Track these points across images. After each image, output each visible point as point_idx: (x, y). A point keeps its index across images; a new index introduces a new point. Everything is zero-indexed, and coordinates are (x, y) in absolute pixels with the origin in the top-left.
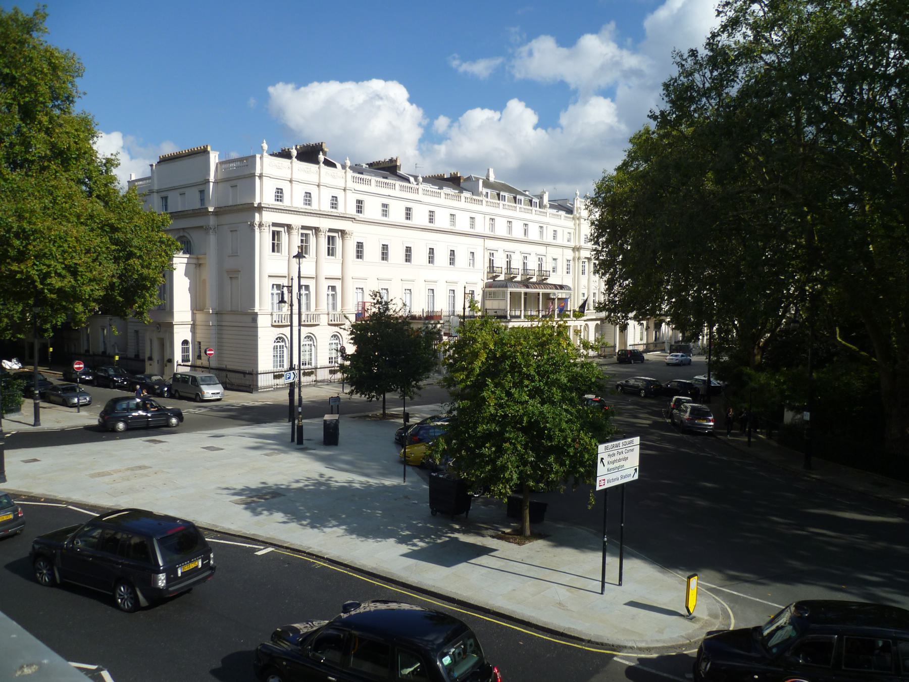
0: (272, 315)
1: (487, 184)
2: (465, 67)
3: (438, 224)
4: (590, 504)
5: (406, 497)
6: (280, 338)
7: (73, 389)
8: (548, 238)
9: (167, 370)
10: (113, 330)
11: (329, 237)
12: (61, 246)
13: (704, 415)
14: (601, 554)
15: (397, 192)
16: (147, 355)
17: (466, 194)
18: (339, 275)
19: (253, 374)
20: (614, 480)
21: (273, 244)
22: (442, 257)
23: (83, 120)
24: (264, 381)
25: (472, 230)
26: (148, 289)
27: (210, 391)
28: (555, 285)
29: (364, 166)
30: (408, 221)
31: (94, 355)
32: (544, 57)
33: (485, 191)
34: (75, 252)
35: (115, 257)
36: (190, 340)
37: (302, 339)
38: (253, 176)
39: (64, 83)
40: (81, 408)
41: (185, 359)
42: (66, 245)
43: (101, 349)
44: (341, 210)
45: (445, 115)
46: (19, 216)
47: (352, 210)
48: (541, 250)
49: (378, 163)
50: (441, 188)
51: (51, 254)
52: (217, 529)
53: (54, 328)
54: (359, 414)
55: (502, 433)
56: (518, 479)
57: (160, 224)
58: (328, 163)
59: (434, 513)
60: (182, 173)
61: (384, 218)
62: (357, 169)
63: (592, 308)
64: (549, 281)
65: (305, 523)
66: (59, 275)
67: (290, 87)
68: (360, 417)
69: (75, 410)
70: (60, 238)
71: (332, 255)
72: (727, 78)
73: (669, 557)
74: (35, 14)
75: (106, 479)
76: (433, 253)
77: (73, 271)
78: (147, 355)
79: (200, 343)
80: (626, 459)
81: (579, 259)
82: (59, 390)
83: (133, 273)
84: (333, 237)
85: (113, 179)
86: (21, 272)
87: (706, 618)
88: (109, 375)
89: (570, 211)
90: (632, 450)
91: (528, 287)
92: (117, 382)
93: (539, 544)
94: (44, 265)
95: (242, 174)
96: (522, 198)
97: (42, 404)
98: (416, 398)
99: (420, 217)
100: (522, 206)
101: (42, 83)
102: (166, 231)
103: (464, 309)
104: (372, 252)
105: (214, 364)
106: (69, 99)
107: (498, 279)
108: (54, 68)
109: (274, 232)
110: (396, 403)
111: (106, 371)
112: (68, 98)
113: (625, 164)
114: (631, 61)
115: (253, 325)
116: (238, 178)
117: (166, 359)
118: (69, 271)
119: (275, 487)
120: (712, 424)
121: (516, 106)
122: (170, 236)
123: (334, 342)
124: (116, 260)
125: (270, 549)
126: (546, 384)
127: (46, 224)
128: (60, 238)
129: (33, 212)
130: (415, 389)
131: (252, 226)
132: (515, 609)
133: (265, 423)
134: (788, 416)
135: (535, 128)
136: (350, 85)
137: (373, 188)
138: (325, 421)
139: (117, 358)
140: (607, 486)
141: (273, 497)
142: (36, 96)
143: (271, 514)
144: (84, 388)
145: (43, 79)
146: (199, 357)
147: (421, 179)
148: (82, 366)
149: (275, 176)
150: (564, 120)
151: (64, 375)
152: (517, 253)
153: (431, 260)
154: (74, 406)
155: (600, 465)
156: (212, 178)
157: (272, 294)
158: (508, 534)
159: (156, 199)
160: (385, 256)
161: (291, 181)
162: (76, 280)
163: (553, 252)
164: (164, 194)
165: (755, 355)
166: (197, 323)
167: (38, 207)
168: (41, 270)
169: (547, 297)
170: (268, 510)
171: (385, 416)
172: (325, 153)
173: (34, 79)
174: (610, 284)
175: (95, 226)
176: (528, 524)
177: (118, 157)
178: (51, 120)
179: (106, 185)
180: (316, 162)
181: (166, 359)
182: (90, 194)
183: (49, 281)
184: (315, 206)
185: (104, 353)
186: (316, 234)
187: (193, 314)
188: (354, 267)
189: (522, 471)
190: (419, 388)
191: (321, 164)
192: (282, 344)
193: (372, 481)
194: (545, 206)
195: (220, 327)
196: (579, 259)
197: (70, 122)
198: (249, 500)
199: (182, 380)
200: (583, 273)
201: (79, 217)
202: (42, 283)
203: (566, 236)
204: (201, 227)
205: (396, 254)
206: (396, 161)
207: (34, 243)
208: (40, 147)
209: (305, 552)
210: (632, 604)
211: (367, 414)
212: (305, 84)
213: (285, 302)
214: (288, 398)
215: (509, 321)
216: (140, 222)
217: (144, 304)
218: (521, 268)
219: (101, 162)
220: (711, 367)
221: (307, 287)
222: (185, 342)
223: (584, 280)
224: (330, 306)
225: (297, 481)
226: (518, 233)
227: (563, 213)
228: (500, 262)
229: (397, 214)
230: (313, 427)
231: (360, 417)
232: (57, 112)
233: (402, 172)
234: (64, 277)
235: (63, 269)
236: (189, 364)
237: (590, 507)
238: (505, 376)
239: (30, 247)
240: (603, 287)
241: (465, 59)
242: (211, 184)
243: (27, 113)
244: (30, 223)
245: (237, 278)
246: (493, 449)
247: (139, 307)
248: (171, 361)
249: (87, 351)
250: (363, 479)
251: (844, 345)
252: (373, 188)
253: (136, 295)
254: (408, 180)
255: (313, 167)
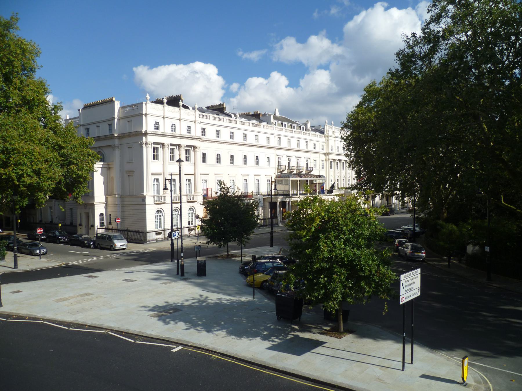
0: (154, 197)
1: (275, 118)
2: (246, 56)
3: (248, 141)
4: (385, 311)
5: (258, 309)
6: (159, 211)
7: (36, 245)
8: (311, 148)
9: (91, 231)
10: (59, 208)
11: (186, 150)
12: (30, 158)
13: (419, 250)
14: (401, 345)
15: (225, 123)
16: (79, 223)
17: (264, 124)
18: (193, 172)
19: (144, 233)
20: (409, 297)
21: (154, 155)
22: (251, 160)
23: (41, 82)
24: (150, 237)
25: (268, 144)
26: (81, 183)
27: (119, 244)
28: (316, 175)
29: (204, 108)
30: (231, 140)
31: (46, 223)
32: (290, 49)
33: (274, 122)
34: (39, 161)
35: (61, 165)
36: (104, 213)
37: (172, 210)
38: (141, 115)
39: (29, 60)
40: (42, 256)
41: (102, 225)
42: (33, 157)
43: (49, 220)
44: (193, 134)
45: (236, 82)
46: (4, 140)
47: (199, 134)
48: (307, 155)
49: (212, 106)
50: (249, 120)
51: (24, 163)
52: (144, 335)
53: (21, 208)
54: (213, 255)
55: (331, 267)
56: (341, 298)
57: (88, 144)
58: (185, 107)
59: (279, 319)
60: (97, 114)
61: (218, 139)
62: (201, 110)
63: (336, 188)
64: (312, 173)
65: (198, 328)
66: (29, 176)
67: (146, 67)
68: (213, 257)
69: (38, 257)
70: (30, 153)
71: (188, 161)
72: (434, 50)
73: (435, 343)
74: (12, 18)
75: (66, 303)
76: (246, 158)
77: (38, 173)
78: (79, 223)
79: (110, 215)
80: (414, 283)
81: (328, 160)
82: (27, 245)
83: (72, 174)
84: (189, 150)
85: (58, 118)
86: (6, 174)
87: (474, 384)
88: (56, 236)
89: (322, 132)
90: (417, 277)
91: (301, 177)
92: (61, 239)
93: (349, 338)
94: (20, 169)
95: (134, 113)
96: (296, 125)
97: (19, 255)
98: (247, 245)
99: (238, 137)
100: (296, 130)
101: (16, 60)
102: (91, 148)
103: (271, 190)
104: (211, 158)
105: (120, 228)
106: (32, 70)
107: (284, 173)
108: (24, 51)
109: (154, 148)
110: (235, 248)
111: (54, 233)
112: (31, 69)
113: (361, 104)
114: (337, 50)
115: (143, 203)
116: (132, 116)
117: (90, 225)
118: (35, 173)
119: (174, 305)
120: (424, 255)
121: (275, 76)
122: (93, 151)
123: (190, 212)
124: (62, 166)
125: (180, 348)
126: (354, 237)
127: (21, 145)
128: (30, 153)
129: (12, 137)
130: (246, 240)
131: (141, 144)
132: (351, 384)
133: (156, 262)
134: (470, 249)
135: (286, 87)
136: (181, 66)
137: (211, 121)
138: (198, 261)
139: (60, 225)
140: (406, 301)
141: (175, 312)
142: (13, 68)
143: (176, 323)
144: (42, 244)
145: (16, 57)
146: (110, 223)
147: (238, 115)
148: (42, 231)
149: (154, 115)
150: (302, 83)
151: (28, 236)
152: (303, 158)
153: (245, 162)
154: (37, 255)
155: (401, 288)
156: (116, 116)
157: (154, 185)
158: (328, 331)
159: (82, 129)
160: (218, 160)
161: (163, 118)
162: (40, 179)
163: (314, 156)
164: (87, 127)
165: (443, 213)
166: (109, 203)
167: (15, 134)
168: (18, 173)
169: (311, 181)
170: (174, 320)
171: (228, 256)
172: (182, 101)
173: (12, 57)
174: (358, 173)
175: (49, 146)
176: (342, 324)
177: (62, 105)
178: (21, 82)
179: (55, 121)
180: (178, 106)
181: (90, 225)
182: (45, 127)
183: (23, 179)
184: (178, 132)
185: (51, 222)
186: (179, 148)
187: (106, 198)
188: (202, 168)
189: (344, 292)
190: (249, 239)
191: (181, 107)
192: (160, 214)
193: (234, 299)
194: (308, 130)
195: (122, 205)
196: (328, 160)
197: (34, 83)
198: (160, 314)
199: (102, 237)
200: (331, 168)
201: (40, 140)
202: (18, 181)
203: (321, 147)
204: (110, 146)
205: (225, 159)
206: (223, 105)
207: (14, 156)
208: (15, 99)
209: (203, 349)
210: (424, 376)
211: (217, 255)
212: (156, 66)
213: (167, 189)
214: (170, 246)
215: (291, 197)
216: (76, 143)
217: (79, 192)
218: (296, 166)
219: (51, 108)
220: (416, 220)
221: (174, 180)
222: (102, 215)
223: (331, 172)
224: (188, 191)
225: (187, 300)
226: (294, 146)
227: (318, 134)
228: (284, 163)
229: (225, 136)
230: (190, 264)
231: (213, 257)
232: (24, 78)
233: (227, 111)
234: (32, 177)
235: (32, 172)
236: (104, 227)
237: (384, 313)
238: (330, 232)
239: (11, 159)
240: (354, 176)
241: (245, 51)
242: (116, 120)
243: (7, 79)
244: (10, 144)
245: (132, 175)
246: (326, 279)
247: (77, 194)
248: (93, 226)
249: (41, 221)
250: (228, 297)
251: (507, 206)
252: (211, 121)
253: (75, 186)
254: (231, 116)
255: (176, 109)
